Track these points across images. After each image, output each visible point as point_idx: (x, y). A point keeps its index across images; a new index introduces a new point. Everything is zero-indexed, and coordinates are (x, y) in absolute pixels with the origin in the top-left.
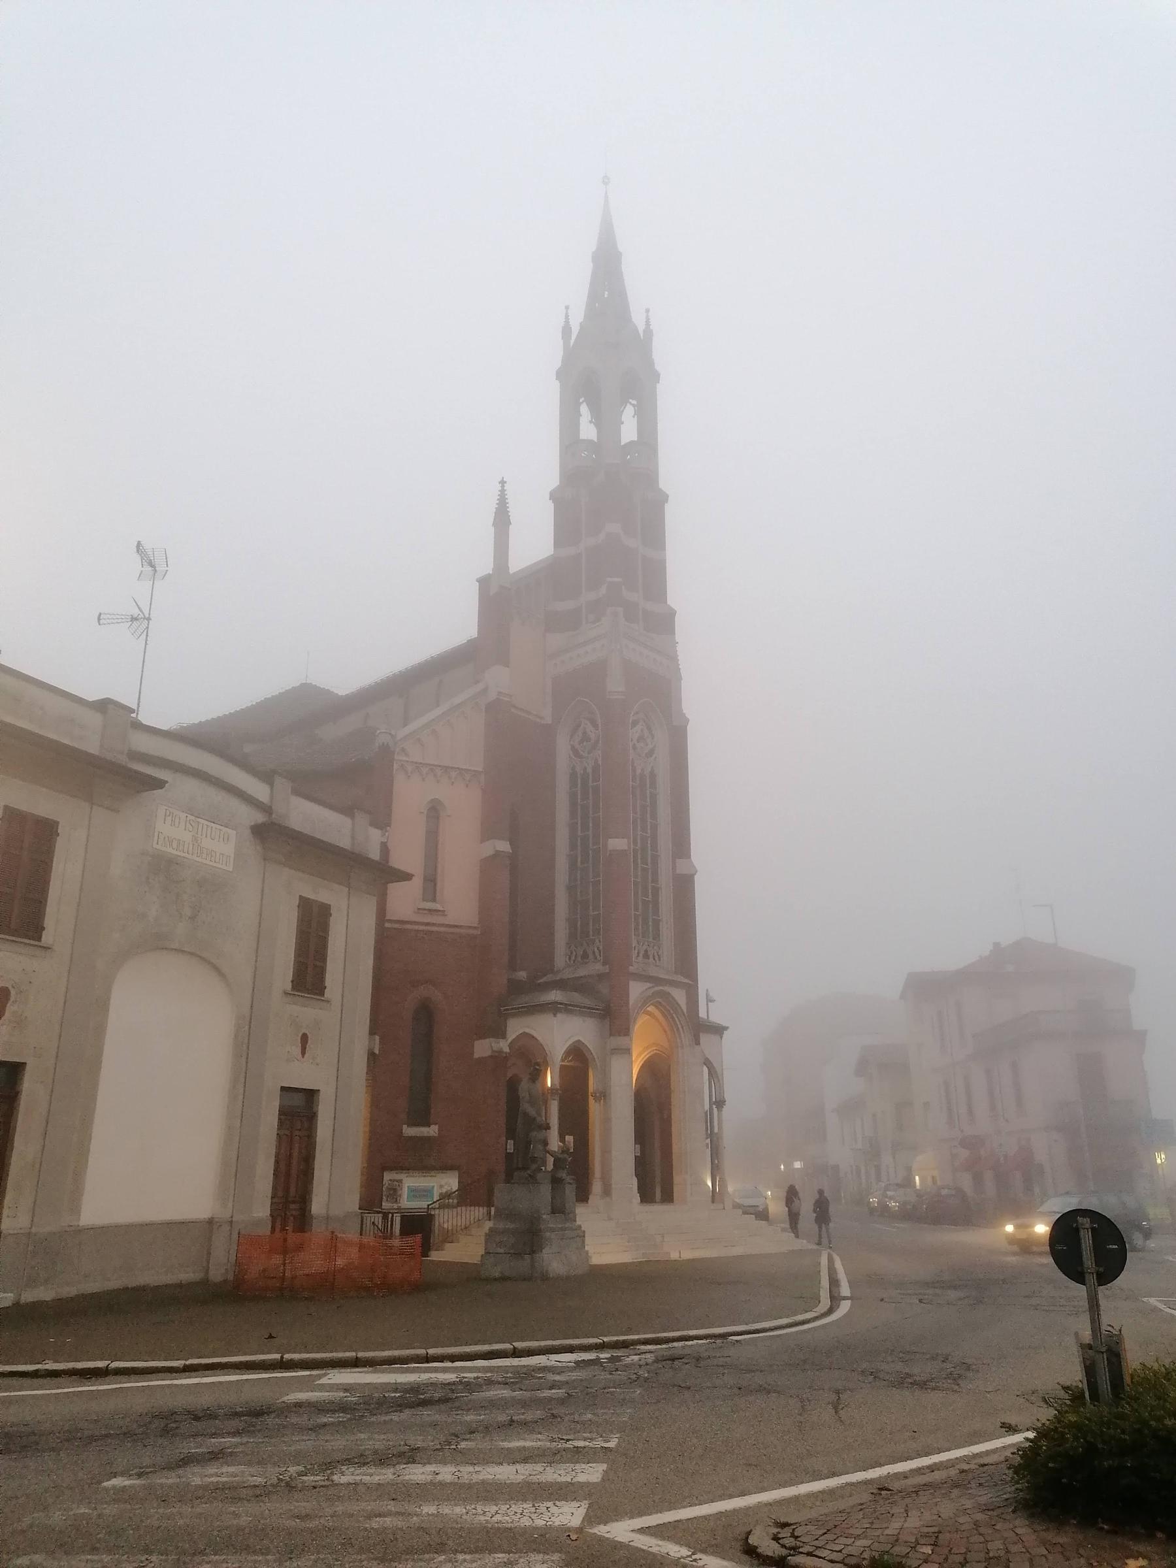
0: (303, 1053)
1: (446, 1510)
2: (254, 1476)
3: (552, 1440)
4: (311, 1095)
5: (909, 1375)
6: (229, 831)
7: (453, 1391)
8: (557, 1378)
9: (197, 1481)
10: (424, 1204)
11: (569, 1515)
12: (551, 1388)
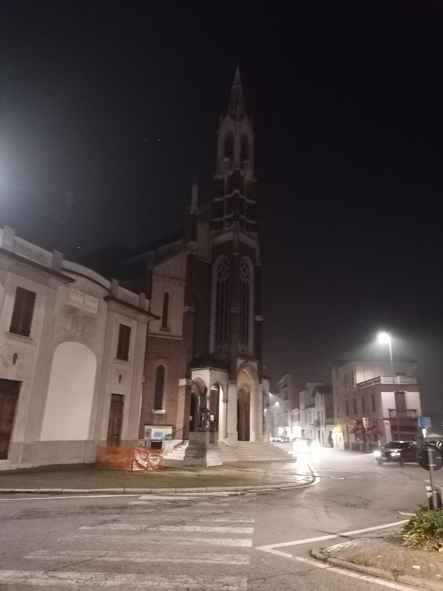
0: (120, 381)
1: (204, 540)
3: (231, 520)
4: (122, 396)
5: (349, 503)
7: (189, 503)
9: (112, 528)
10: (160, 438)
11: (247, 543)
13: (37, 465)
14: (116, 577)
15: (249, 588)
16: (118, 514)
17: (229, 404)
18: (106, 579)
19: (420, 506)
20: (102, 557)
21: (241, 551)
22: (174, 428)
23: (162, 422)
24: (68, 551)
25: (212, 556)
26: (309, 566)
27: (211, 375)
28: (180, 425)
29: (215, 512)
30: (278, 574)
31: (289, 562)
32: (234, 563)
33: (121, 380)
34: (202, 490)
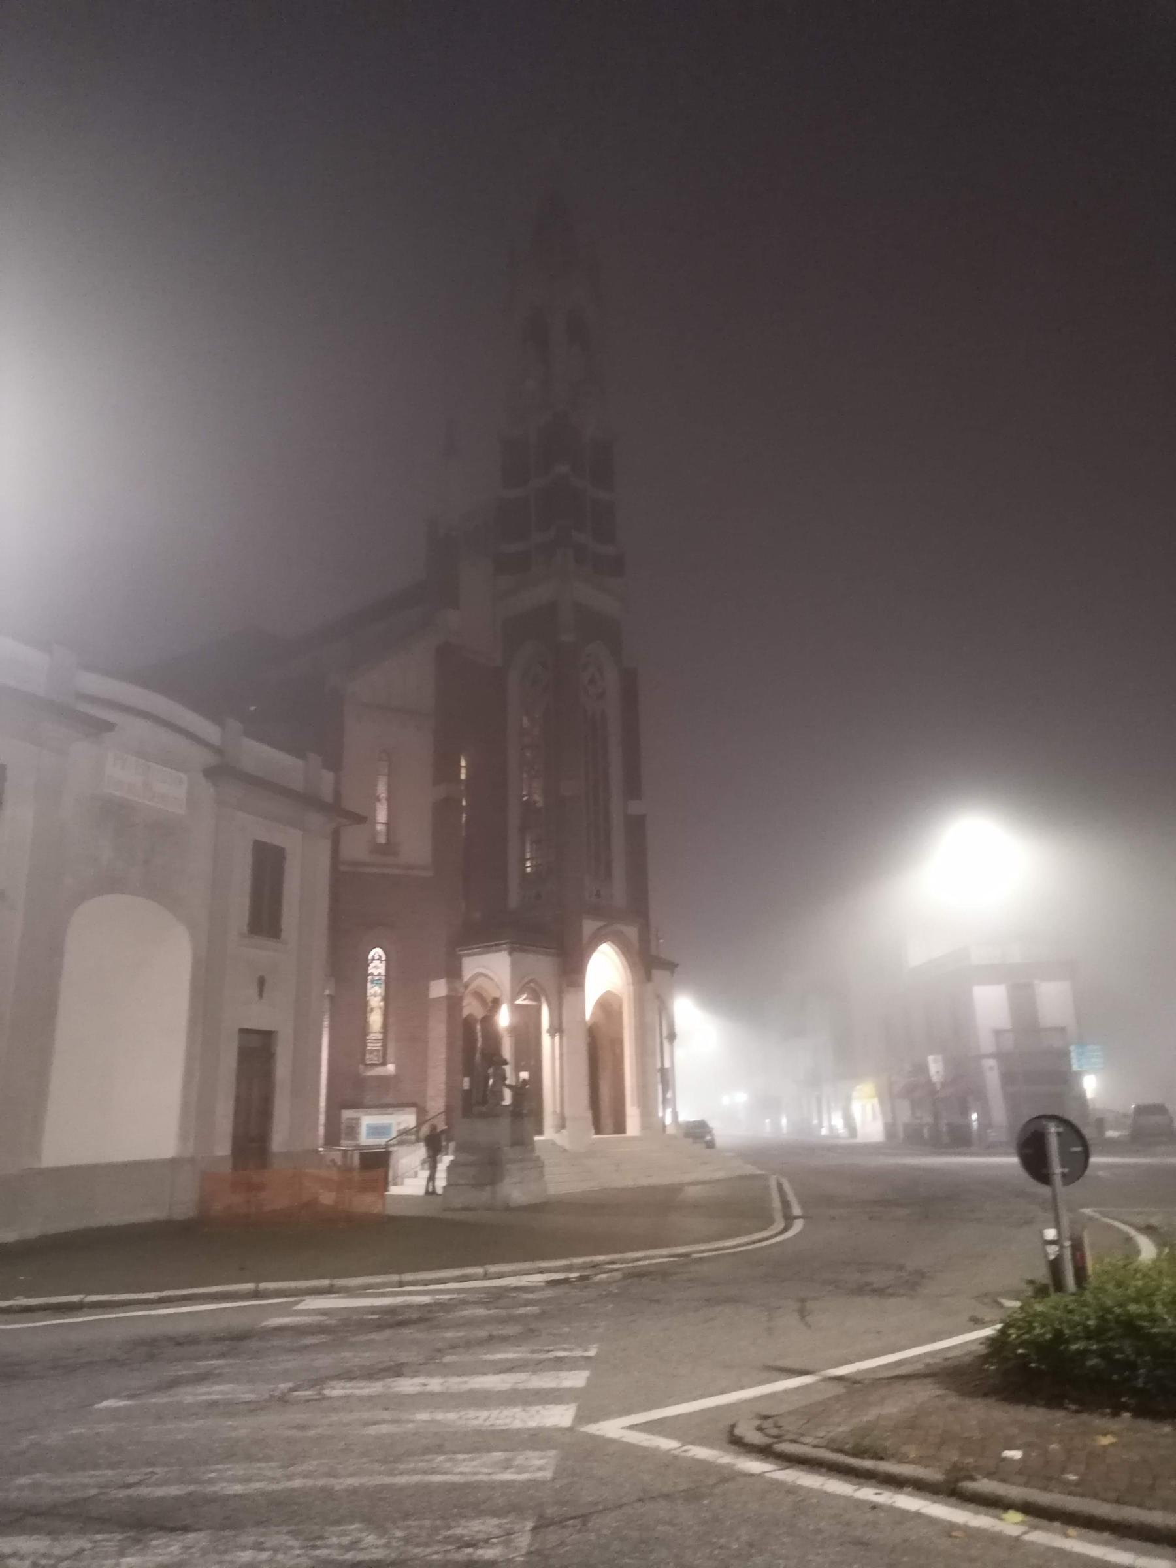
0: (261, 994)
1: (440, 1416)
2: (245, 1393)
3: (533, 1352)
4: (267, 1037)
5: (868, 1284)
6: (182, 775)
7: (429, 1311)
8: (530, 1296)
9: (189, 1399)
10: (382, 1141)
11: (560, 1416)
12: (526, 1306)
13: (32, 1231)
14: (154, 1543)
15: (532, 1549)
16: (222, 1355)
17: (565, 1039)
18: (122, 1553)
19: (1031, 1282)
20: (129, 1486)
21: (537, 1439)
22: (421, 1113)
23: (386, 1096)
24: (37, 1475)
25: (450, 1460)
26: (718, 1468)
27: (514, 966)
28: (436, 1104)
29: (495, 1333)
30: (625, 1500)
31: (670, 1462)
32: (507, 1476)
33: (265, 995)
34: (475, 1274)
